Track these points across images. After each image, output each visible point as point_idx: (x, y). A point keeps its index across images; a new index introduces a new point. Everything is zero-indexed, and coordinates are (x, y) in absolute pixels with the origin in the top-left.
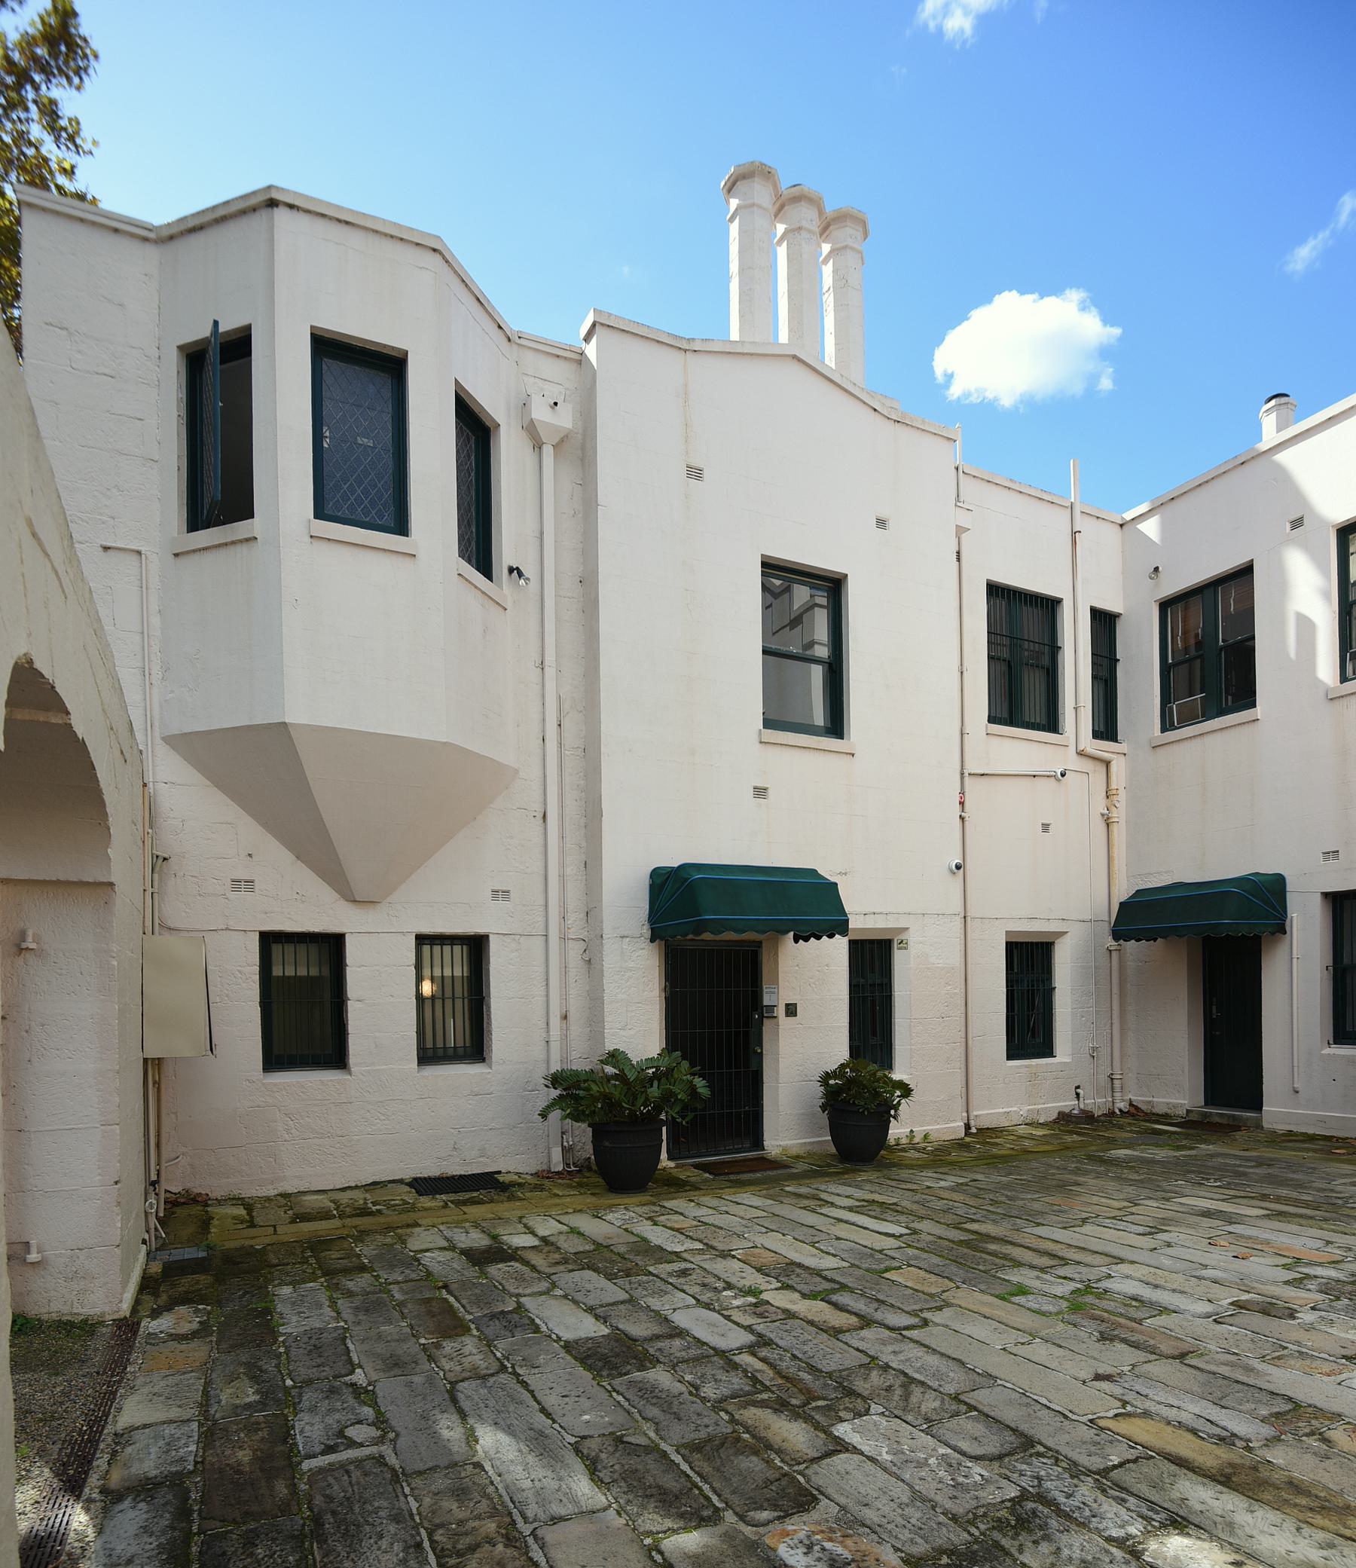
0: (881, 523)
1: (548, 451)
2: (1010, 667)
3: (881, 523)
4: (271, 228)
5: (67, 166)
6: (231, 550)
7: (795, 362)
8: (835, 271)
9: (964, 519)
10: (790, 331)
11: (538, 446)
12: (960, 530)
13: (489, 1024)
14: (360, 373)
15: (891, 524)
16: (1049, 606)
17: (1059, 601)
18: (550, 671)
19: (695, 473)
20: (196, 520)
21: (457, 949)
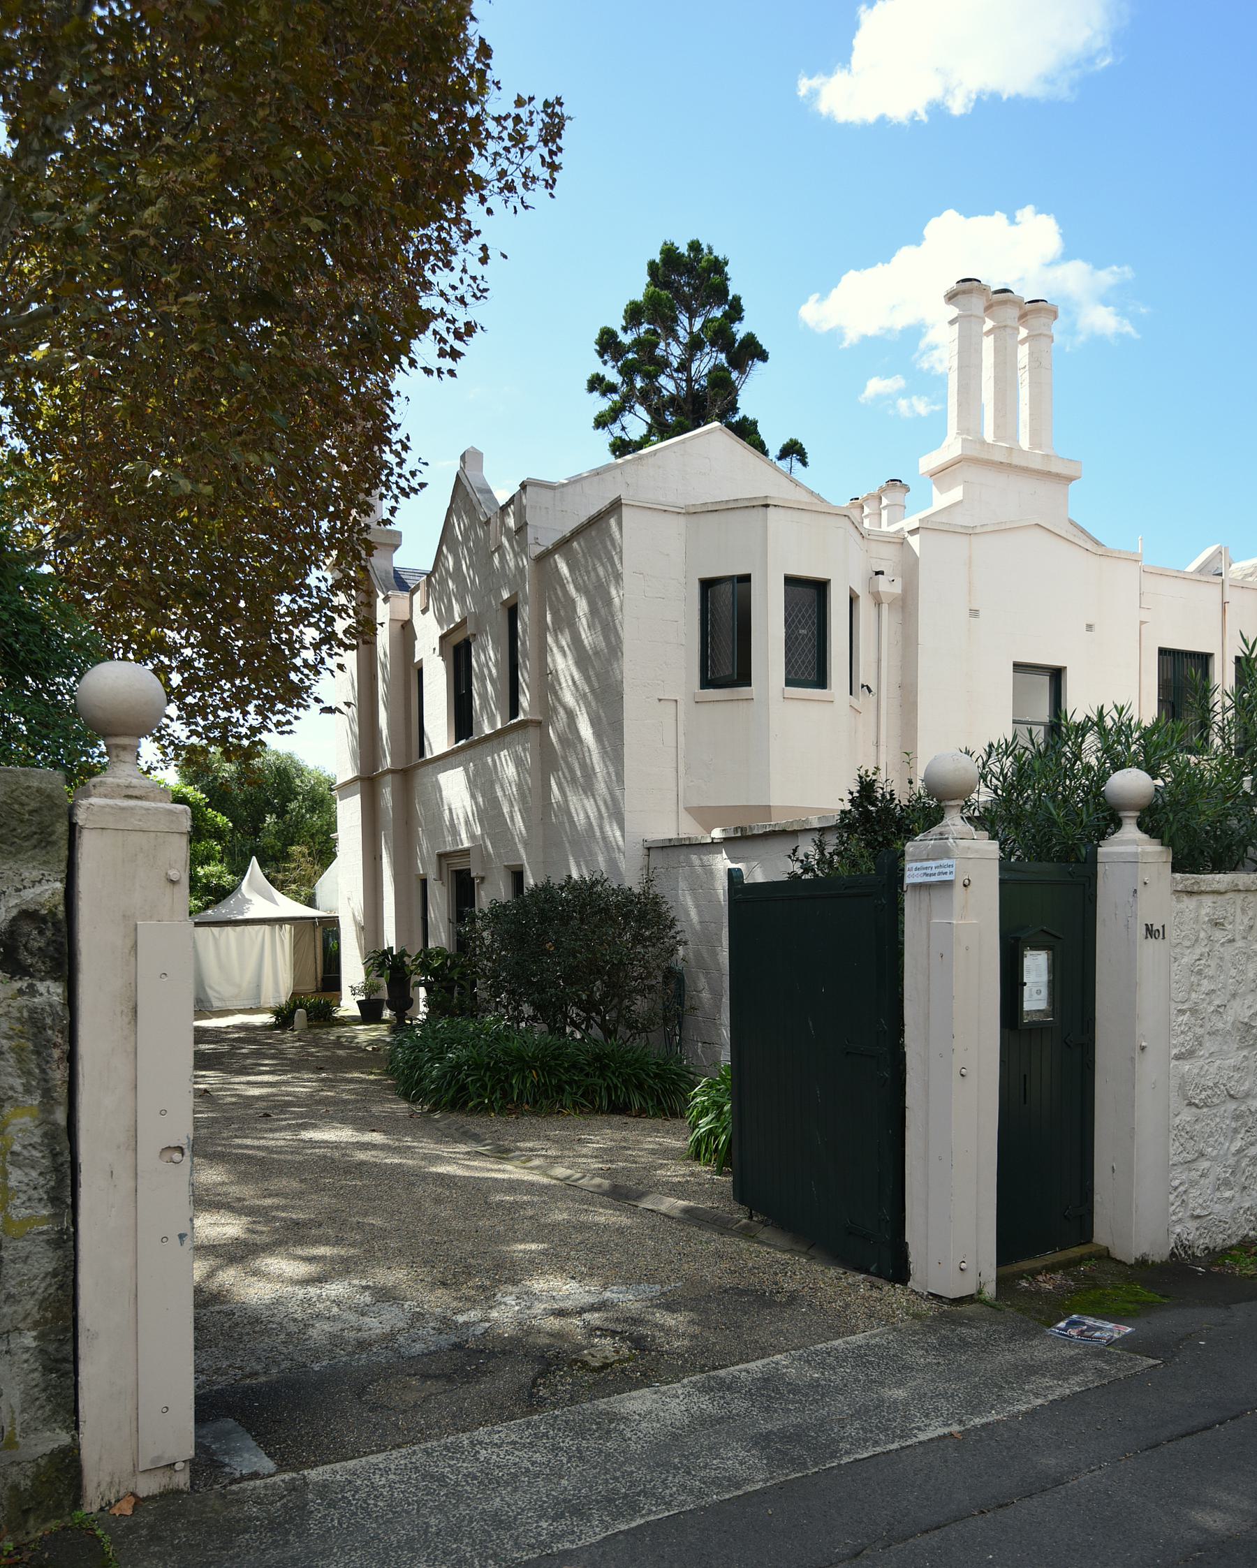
0: (1090, 627)
1: (885, 607)
2: (1173, 707)
3: (1090, 627)
4: (766, 520)
5: (460, 324)
6: (735, 703)
7: (1038, 530)
8: (1031, 354)
9: (1145, 615)
10: (996, 410)
11: (879, 604)
12: (1142, 623)
13: (80, 1068)
14: (808, 595)
15: (1096, 628)
16: (1204, 660)
17: (1211, 655)
18: (883, 748)
19: (974, 613)
20: (707, 682)
21: (288, 927)
